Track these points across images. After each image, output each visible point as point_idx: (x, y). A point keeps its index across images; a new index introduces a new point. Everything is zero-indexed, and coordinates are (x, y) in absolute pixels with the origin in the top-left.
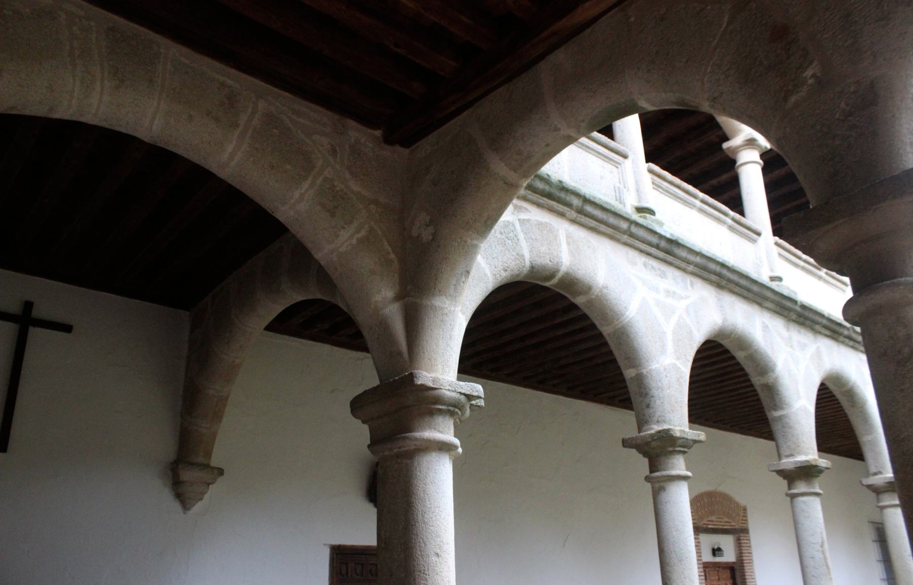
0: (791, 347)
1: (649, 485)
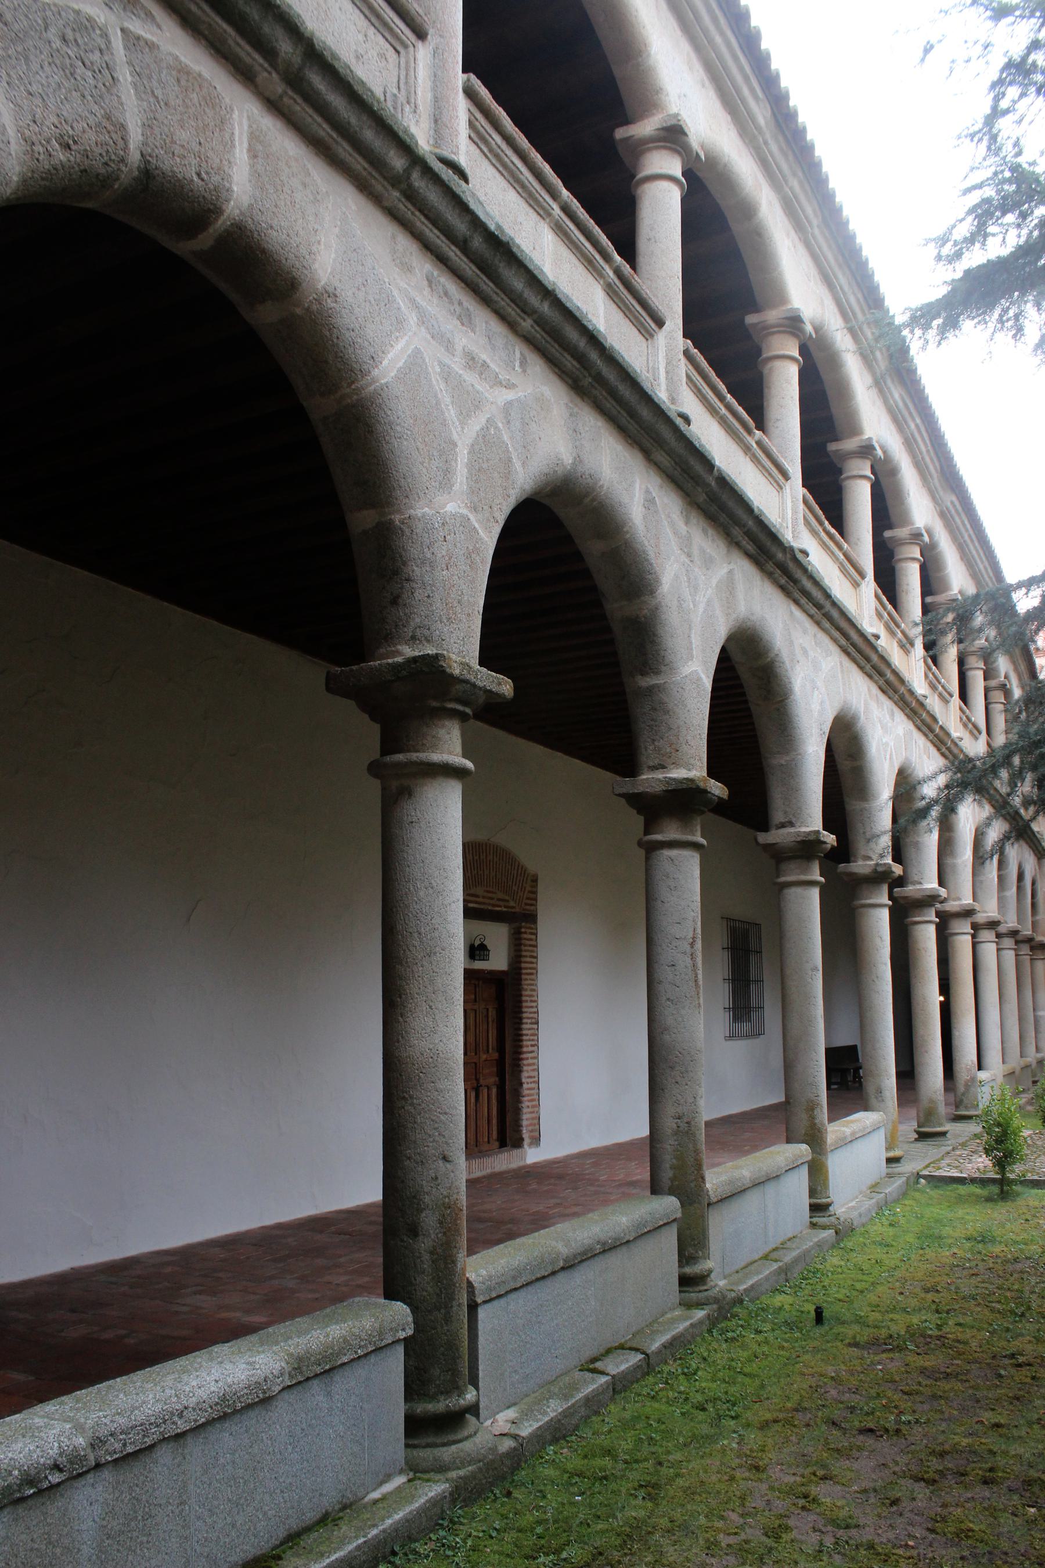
0: (689, 555)
1: (377, 784)
